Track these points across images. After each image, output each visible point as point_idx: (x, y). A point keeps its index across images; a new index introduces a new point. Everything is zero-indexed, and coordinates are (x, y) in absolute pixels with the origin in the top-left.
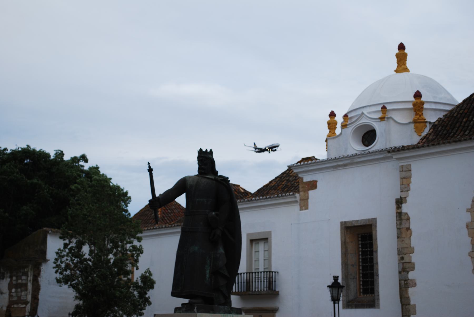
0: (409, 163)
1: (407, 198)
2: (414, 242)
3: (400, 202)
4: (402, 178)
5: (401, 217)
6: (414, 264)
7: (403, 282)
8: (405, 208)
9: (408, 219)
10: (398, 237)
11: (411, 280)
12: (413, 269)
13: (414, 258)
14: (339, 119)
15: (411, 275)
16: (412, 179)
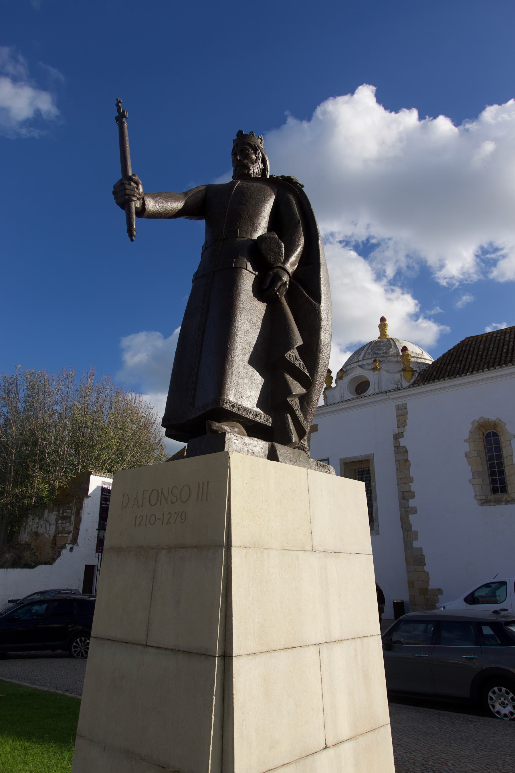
0: (404, 402)
1: (404, 433)
2: (413, 472)
3: (397, 437)
4: (398, 416)
5: (401, 452)
6: (414, 492)
7: (403, 509)
8: (402, 442)
9: (406, 451)
10: (397, 469)
11: (411, 508)
12: (413, 497)
13: (414, 487)
14: (334, 375)
15: (412, 503)
16: (409, 416)
